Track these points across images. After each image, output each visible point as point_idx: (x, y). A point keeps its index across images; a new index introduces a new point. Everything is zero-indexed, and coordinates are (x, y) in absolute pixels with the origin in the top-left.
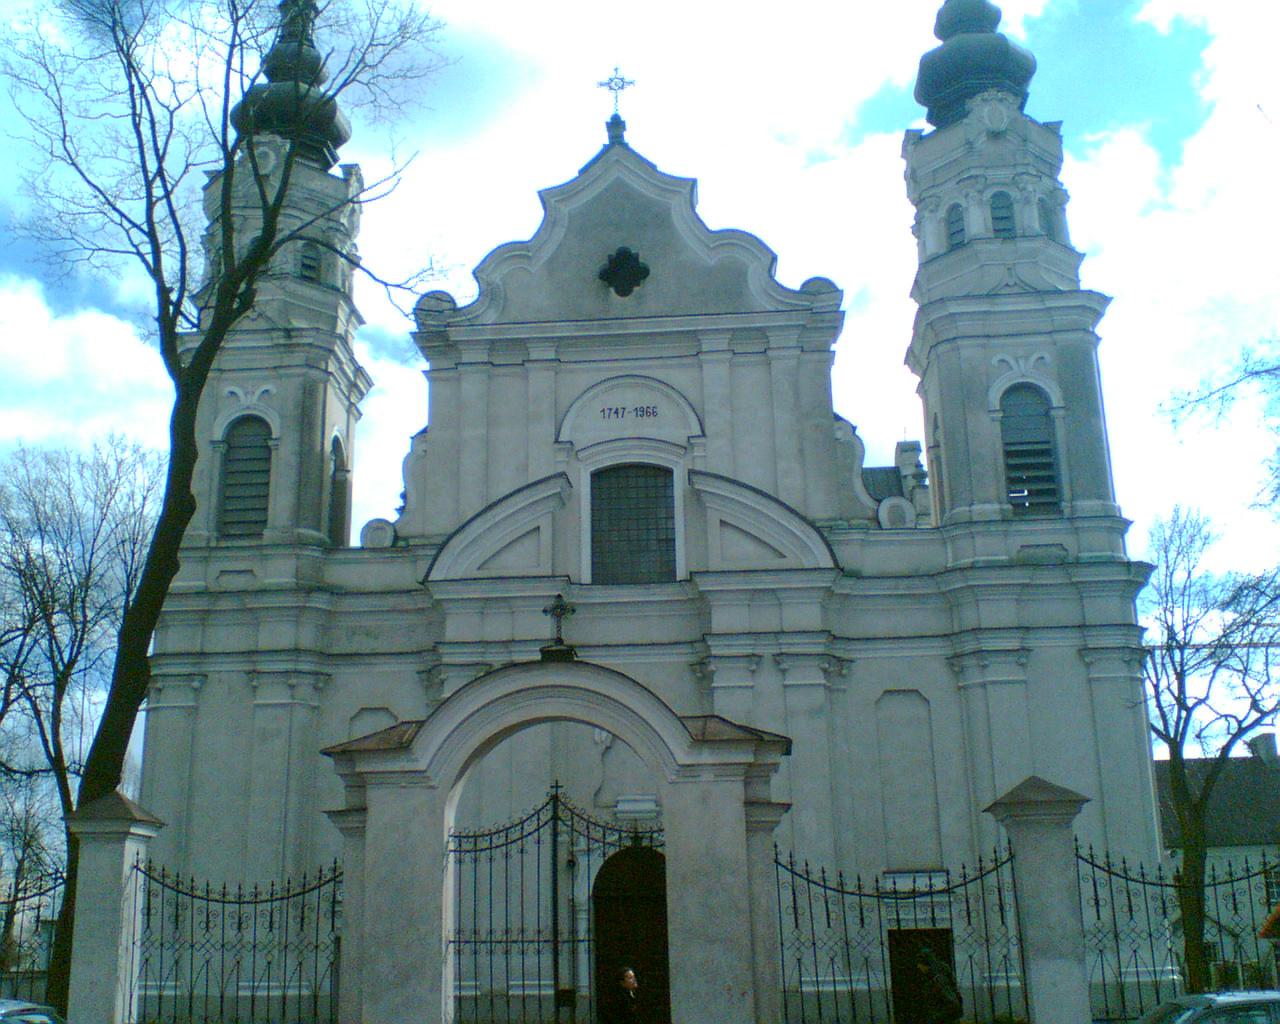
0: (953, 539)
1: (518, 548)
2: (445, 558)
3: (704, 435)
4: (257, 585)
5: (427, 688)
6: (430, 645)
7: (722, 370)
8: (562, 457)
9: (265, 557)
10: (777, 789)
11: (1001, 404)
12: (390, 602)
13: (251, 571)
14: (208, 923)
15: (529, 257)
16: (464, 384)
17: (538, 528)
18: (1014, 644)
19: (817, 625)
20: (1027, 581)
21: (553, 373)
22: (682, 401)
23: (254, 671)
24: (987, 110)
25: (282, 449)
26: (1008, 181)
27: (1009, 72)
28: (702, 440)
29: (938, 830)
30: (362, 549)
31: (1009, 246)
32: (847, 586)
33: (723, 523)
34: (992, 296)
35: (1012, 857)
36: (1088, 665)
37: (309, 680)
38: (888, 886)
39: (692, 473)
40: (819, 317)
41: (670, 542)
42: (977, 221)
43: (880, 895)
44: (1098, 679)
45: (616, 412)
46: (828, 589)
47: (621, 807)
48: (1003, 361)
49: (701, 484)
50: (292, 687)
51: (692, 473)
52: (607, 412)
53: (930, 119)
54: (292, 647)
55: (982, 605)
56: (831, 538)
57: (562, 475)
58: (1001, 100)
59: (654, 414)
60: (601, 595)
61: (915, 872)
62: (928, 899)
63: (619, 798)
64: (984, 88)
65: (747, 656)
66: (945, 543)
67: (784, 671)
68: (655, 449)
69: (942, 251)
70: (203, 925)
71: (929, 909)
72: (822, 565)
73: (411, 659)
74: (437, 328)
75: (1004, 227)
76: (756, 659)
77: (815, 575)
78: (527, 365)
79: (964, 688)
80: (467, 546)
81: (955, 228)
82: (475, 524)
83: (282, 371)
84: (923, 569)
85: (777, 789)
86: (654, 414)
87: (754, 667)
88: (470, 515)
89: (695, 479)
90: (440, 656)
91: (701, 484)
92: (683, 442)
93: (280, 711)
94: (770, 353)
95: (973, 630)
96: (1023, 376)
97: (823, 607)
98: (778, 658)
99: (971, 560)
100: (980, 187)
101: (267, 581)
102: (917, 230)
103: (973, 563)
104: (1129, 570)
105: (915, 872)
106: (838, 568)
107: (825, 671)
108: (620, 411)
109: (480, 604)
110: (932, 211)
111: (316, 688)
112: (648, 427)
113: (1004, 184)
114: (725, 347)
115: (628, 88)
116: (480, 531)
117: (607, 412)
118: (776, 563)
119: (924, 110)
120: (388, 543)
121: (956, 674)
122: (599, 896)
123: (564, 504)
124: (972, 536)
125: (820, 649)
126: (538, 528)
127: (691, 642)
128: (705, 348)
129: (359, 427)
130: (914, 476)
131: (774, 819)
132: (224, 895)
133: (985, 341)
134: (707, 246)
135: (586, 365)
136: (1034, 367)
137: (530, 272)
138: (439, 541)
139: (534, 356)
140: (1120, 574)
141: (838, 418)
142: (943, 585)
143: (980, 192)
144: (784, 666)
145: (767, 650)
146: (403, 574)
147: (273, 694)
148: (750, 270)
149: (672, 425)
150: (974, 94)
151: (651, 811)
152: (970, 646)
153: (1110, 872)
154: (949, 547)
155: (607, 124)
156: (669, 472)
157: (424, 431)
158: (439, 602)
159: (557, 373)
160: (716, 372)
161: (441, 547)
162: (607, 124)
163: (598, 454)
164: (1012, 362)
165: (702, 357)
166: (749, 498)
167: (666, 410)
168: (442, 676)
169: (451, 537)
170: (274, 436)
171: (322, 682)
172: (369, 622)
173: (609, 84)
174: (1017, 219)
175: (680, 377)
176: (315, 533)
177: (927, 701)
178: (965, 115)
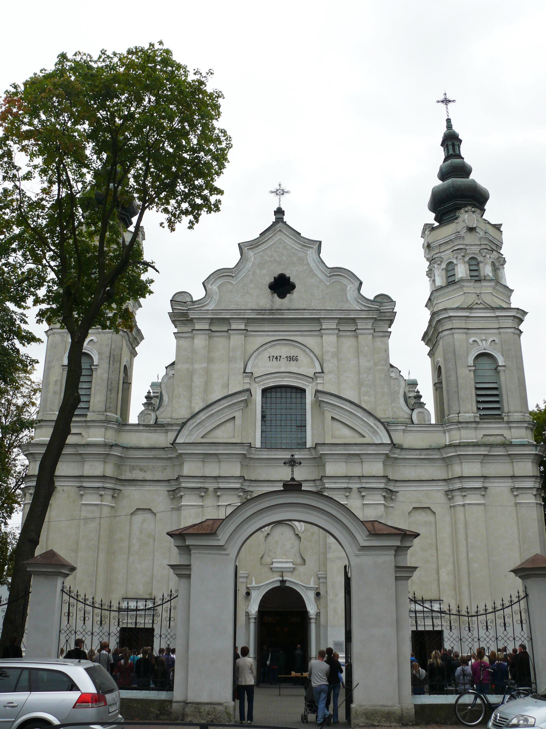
0: (449, 430)
1: (223, 428)
2: (185, 431)
3: (323, 372)
4: (83, 442)
5: (173, 499)
6: (175, 477)
7: (333, 338)
8: (247, 380)
9: (88, 427)
10: (410, 559)
11: (474, 364)
12: (151, 454)
13: (81, 434)
14: (101, 621)
15: (233, 277)
16: (195, 340)
17: (234, 417)
18: (479, 485)
19: (238, 474)
20: (487, 453)
21: (243, 336)
22: (311, 354)
23: (82, 486)
24: (466, 217)
25: (99, 371)
26: (476, 252)
27: (477, 198)
28: (322, 375)
29: (439, 580)
30: (138, 425)
31: (478, 285)
32: (397, 454)
33: (333, 418)
34: (470, 308)
35: (527, 596)
36: (516, 496)
37: (110, 492)
38: (124, 605)
39: (317, 391)
40: (383, 314)
41: (303, 426)
42: (462, 271)
43: (120, 610)
44: (520, 503)
45: (276, 358)
46: (387, 455)
47: (275, 565)
48: (474, 341)
49: (322, 398)
50: (101, 495)
51: (317, 391)
52: (271, 358)
53: (436, 219)
54: (102, 475)
55: (515, 464)
56: (389, 428)
57: (249, 390)
58: (474, 212)
59: (297, 360)
60: (265, 454)
61: (137, 599)
62: (135, 613)
63: (274, 560)
64: (465, 206)
65: (345, 488)
66: (445, 433)
67: (363, 496)
68: (274, 378)
69: (444, 285)
70: (99, 623)
71: (135, 618)
72: (385, 442)
73: (441, 483)
74: (182, 312)
75: (476, 277)
76: (205, 490)
77: (382, 447)
78: (230, 332)
79: (454, 506)
80: (197, 425)
81: (450, 274)
82: (201, 414)
83: (501, 330)
84: (434, 445)
85: (410, 559)
86: (297, 360)
87: (483, 493)
88: (197, 410)
89: (319, 395)
90: (324, 484)
91: (322, 398)
92: (312, 375)
93: (95, 508)
94: (358, 331)
95: (459, 477)
96: (485, 349)
97: (383, 463)
98: (360, 490)
99: (459, 441)
100: (463, 254)
101: (89, 439)
102: (430, 273)
103: (460, 443)
104: (536, 449)
105: (137, 599)
106: (393, 445)
107: (384, 497)
108: (279, 358)
109: (482, 457)
110: (438, 265)
111: (113, 497)
112: (293, 367)
113: (474, 254)
114: (335, 327)
115: (285, 195)
116: (203, 418)
117: (271, 358)
118: (360, 440)
119: (433, 215)
120: (152, 422)
121: (450, 499)
122: (261, 612)
123: (247, 405)
124: (510, 428)
125: (382, 486)
126: (234, 417)
127: (314, 480)
128: (324, 327)
129: (136, 360)
130: (415, 397)
131: (67, 572)
132: (110, 607)
133: (466, 331)
134: (326, 275)
135: (261, 333)
136: (490, 345)
137: (232, 284)
138: (180, 422)
139: (234, 327)
140: (532, 451)
141: (392, 366)
142: (445, 454)
143: (463, 256)
144: (219, 494)
145: (211, 486)
146: (161, 439)
147: (92, 499)
148: (348, 289)
149: (306, 366)
150: (462, 208)
151: (291, 568)
152: (458, 485)
153: (94, 607)
154: (447, 434)
155: (275, 211)
156: (303, 391)
157: (173, 364)
158: (181, 454)
159: (245, 337)
160: (330, 340)
161: (184, 424)
162: (275, 211)
163: (266, 379)
164: (480, 342)
165: (322, 331)
166: (347, 406)
167: (302, 358)
168: (182, 493)
169: (189, 420)
170: (95, 364)
171: (116, 494)
172: (143, 464)
173: (276, 192)
174: (481, 269)
175: (310, 341)
176: (115, 415)
177: (435, 513)
178: (456, 218)
